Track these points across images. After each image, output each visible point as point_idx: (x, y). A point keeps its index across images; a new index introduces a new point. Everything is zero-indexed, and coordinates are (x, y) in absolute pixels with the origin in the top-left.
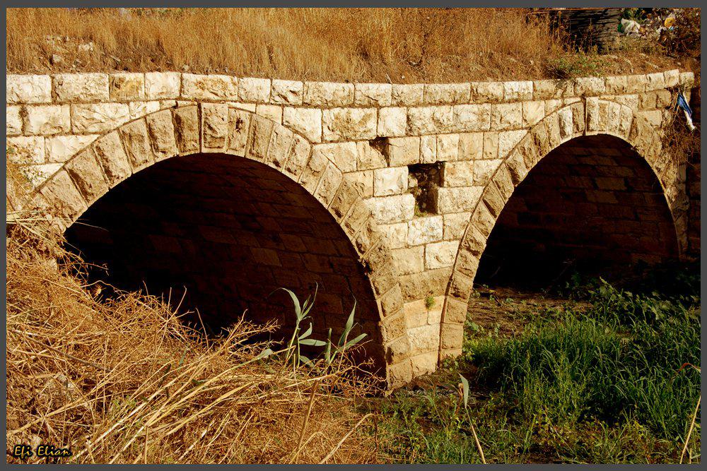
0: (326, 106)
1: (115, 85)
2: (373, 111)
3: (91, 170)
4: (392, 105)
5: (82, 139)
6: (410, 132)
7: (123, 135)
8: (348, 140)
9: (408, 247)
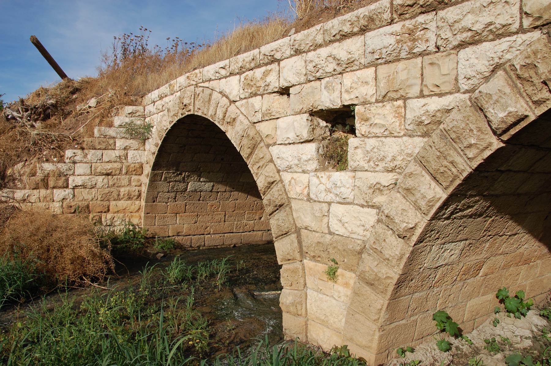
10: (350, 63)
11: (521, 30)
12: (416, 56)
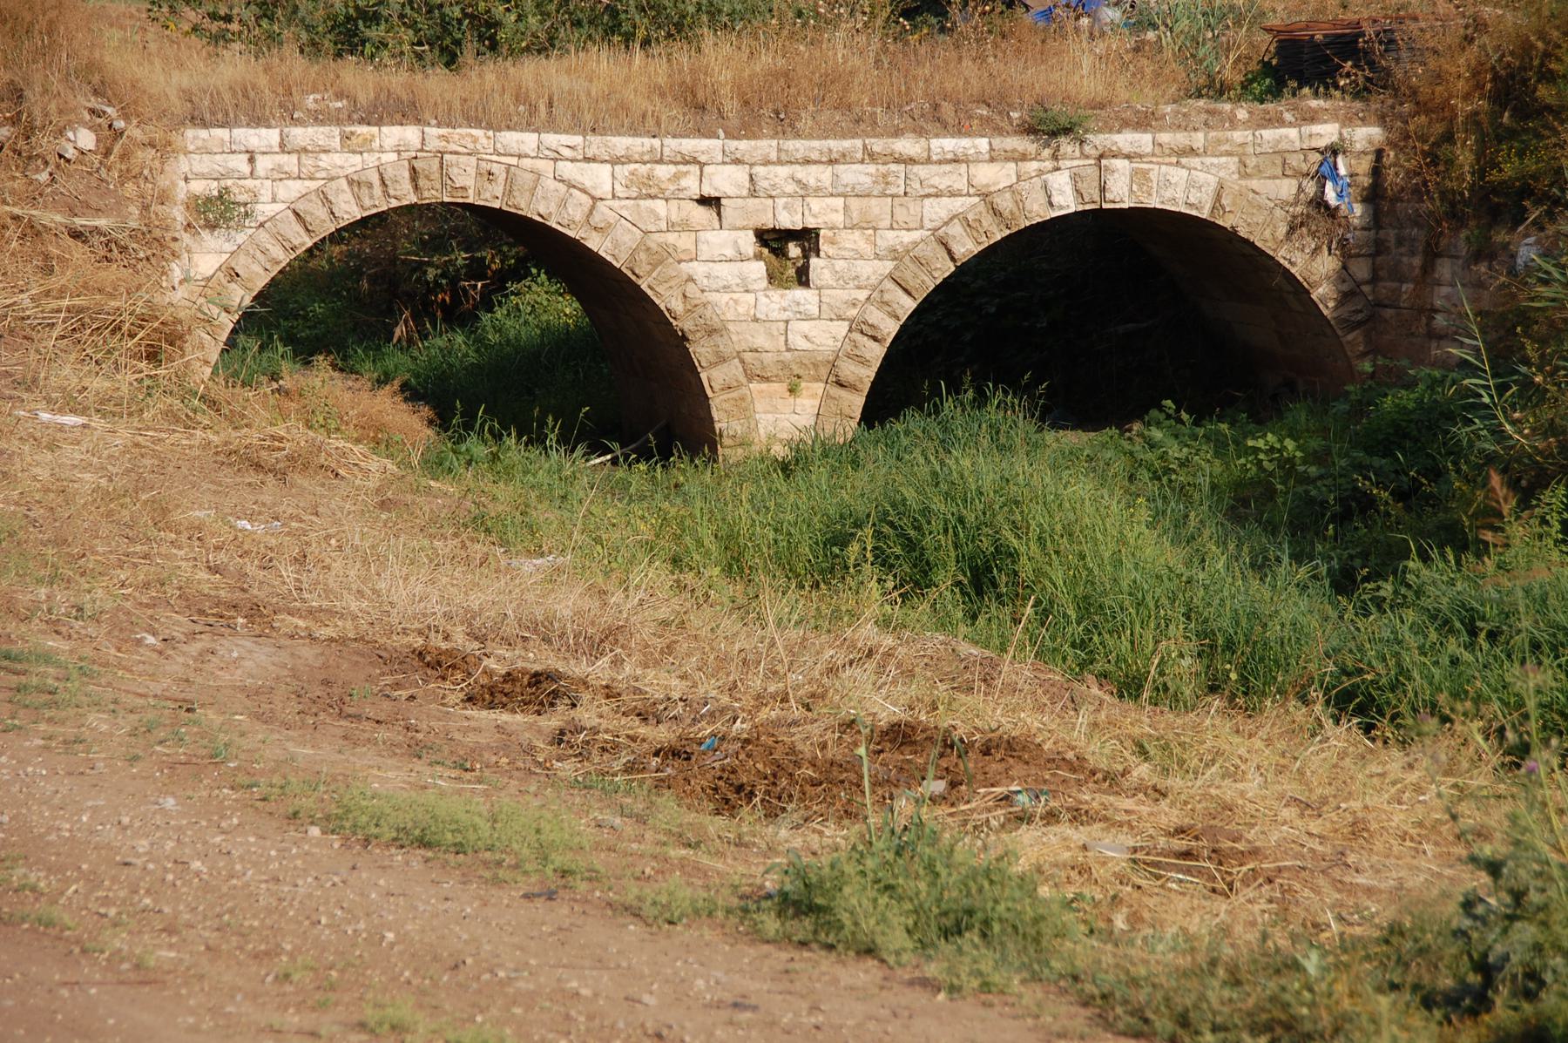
0: (615, 161)
1: (346, 137)
2: (695, 169)
3: (911, 275)
4: (724, 163)
5: (308, 183)
6: (753, 193)
7: (351, 182)
8: (651, 197)
9: (756, 320)
10: (818, 189)
11: (968, 195)
12: (886, 196)
